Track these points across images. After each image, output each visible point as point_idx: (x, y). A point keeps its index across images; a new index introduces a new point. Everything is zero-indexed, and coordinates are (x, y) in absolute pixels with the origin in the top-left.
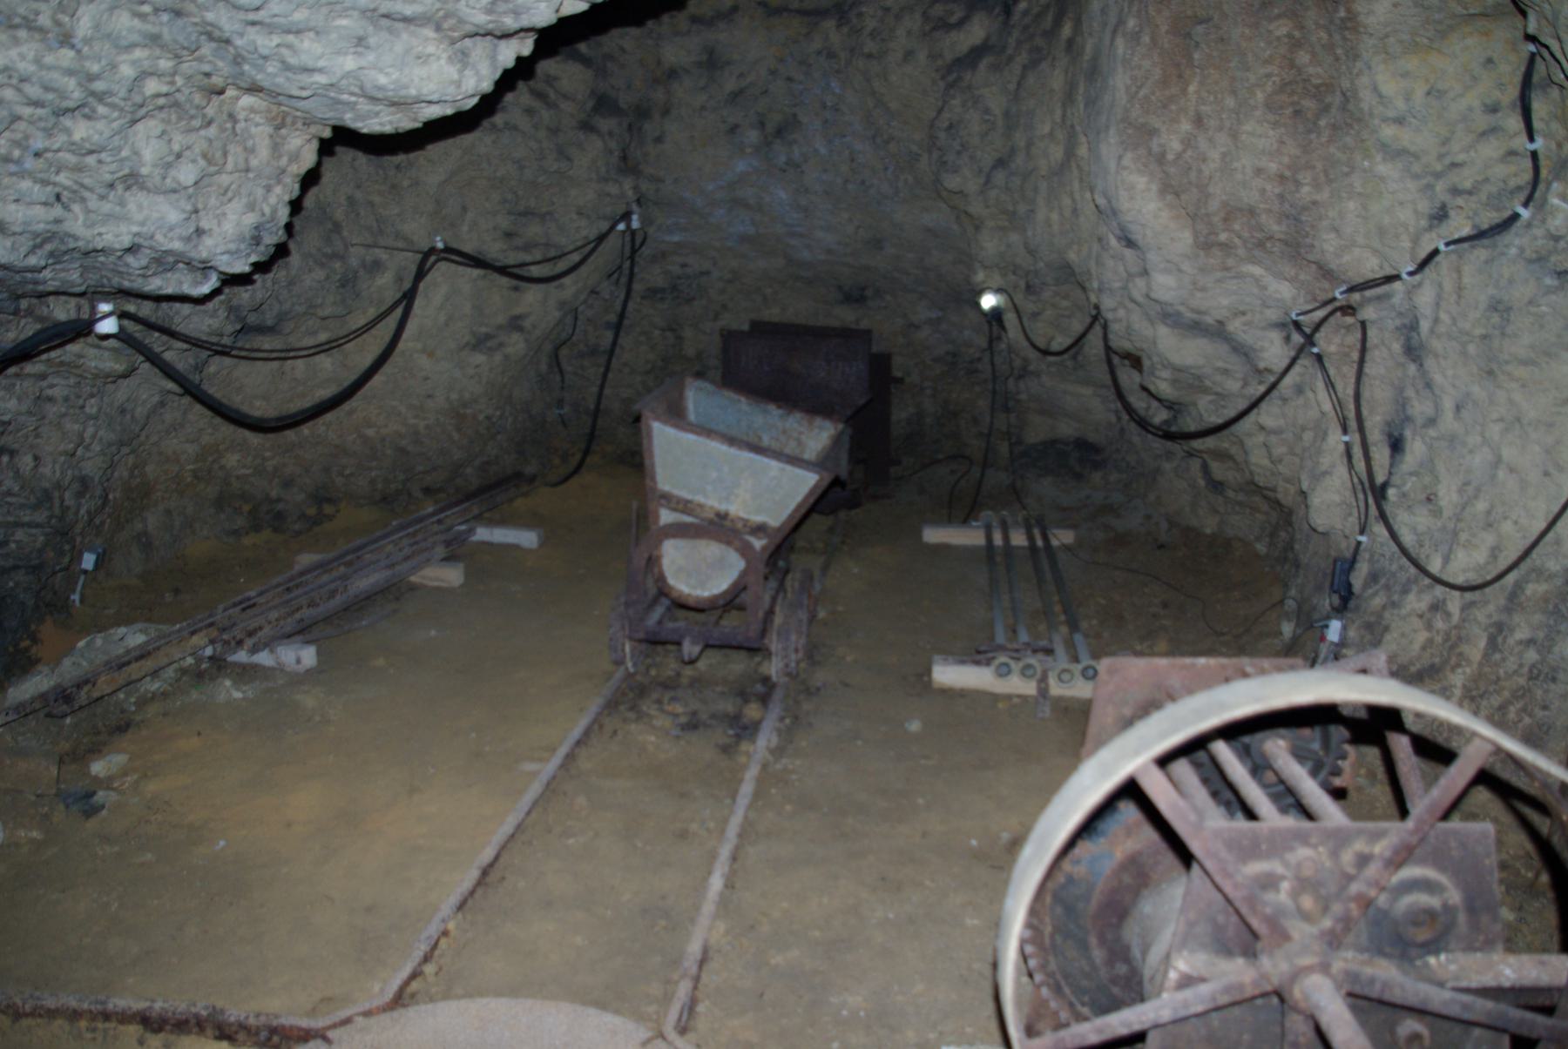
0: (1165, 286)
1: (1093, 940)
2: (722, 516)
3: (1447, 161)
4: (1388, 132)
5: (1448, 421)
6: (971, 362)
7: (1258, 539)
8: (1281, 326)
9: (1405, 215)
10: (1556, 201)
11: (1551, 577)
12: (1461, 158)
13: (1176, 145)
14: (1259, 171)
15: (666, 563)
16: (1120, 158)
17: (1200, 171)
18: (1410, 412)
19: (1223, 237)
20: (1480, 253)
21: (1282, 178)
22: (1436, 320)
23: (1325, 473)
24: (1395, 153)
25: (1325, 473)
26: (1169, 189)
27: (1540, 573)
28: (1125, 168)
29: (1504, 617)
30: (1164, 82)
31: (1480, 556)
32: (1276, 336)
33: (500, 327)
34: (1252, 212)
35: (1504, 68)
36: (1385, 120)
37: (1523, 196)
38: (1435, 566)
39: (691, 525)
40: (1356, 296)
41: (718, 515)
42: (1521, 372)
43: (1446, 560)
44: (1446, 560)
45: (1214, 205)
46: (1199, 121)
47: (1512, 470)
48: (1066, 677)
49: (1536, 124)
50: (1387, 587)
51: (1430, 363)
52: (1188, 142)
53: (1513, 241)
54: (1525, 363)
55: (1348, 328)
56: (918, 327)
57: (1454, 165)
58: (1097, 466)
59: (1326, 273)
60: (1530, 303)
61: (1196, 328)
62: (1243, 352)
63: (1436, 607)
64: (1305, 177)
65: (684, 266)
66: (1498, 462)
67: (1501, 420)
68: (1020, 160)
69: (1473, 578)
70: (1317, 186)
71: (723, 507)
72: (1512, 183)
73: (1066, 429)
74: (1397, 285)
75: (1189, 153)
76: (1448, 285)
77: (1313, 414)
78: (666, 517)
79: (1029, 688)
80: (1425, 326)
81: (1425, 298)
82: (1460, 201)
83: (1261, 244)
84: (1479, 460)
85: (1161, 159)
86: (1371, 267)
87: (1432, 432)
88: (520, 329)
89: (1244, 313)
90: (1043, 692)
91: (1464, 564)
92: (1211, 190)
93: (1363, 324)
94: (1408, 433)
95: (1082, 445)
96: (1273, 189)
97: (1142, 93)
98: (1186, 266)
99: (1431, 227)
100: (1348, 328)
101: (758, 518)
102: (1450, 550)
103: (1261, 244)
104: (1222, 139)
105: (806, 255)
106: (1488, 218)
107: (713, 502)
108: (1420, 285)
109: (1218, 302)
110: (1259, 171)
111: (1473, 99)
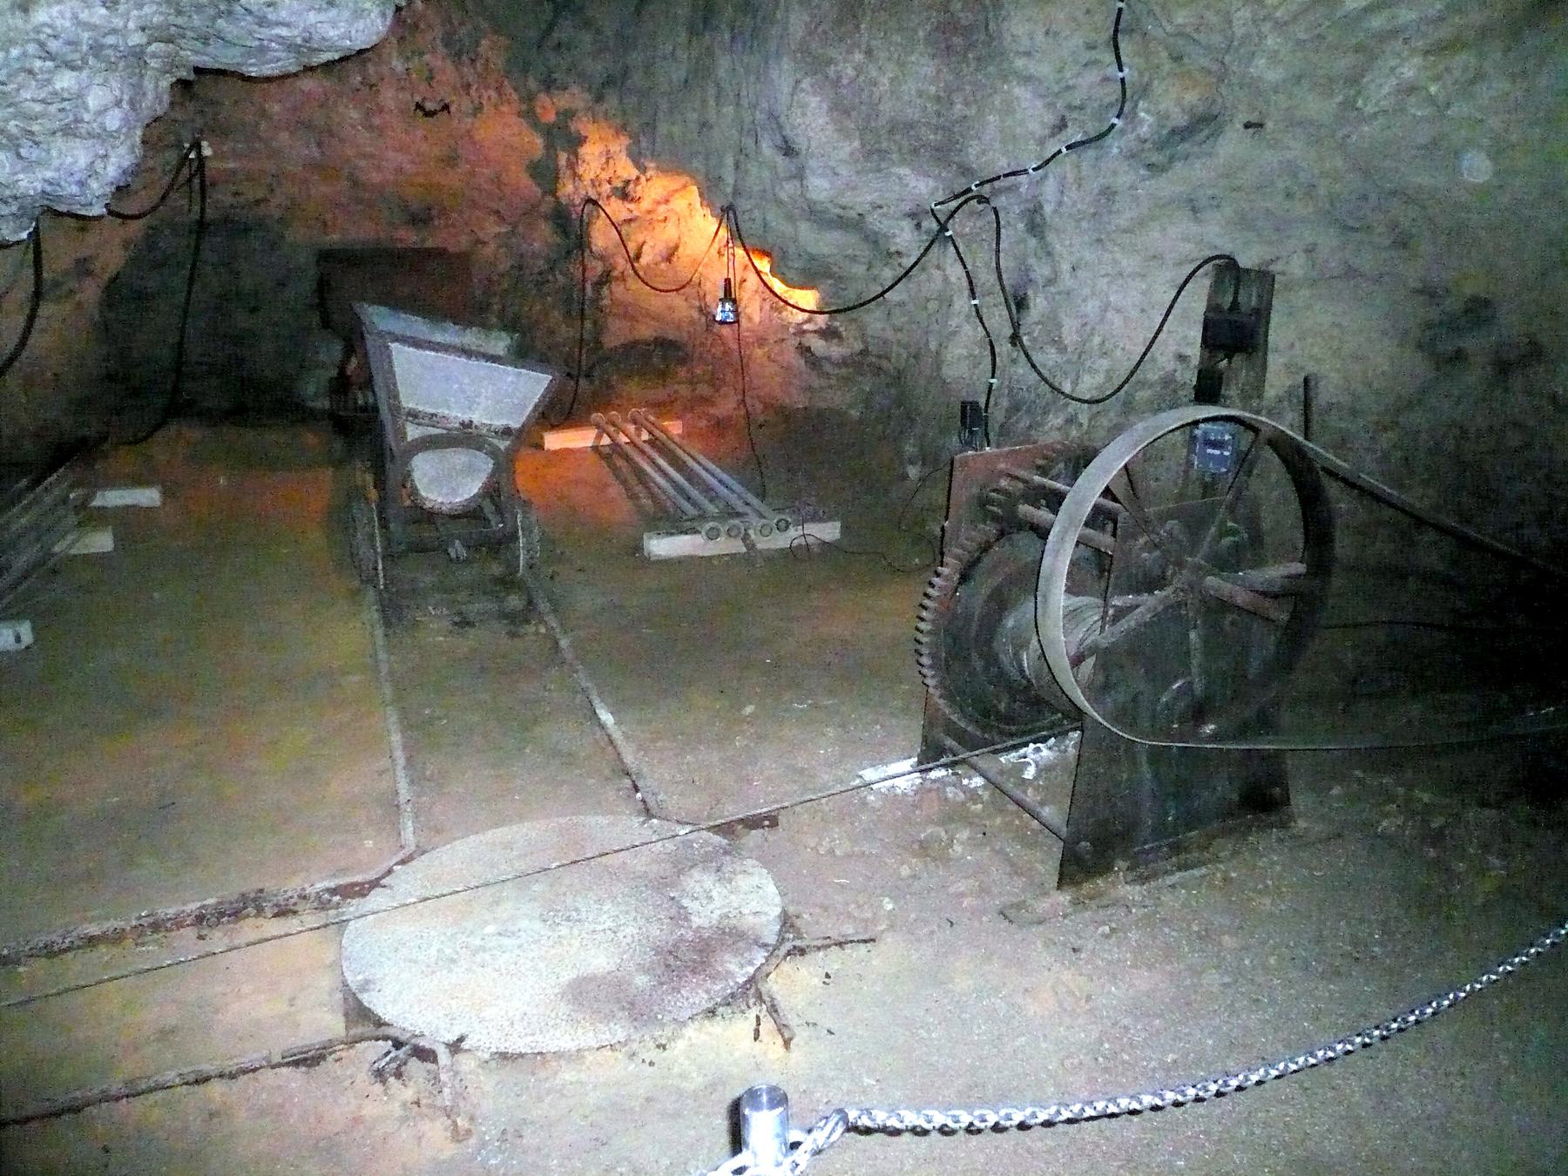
0: (819, 187)
1: (974, 656)
2: (467, 425)
3: (1063, 85)
4: (1020, 63)
5: (1067, 281)
6: (540, 273)
7: (851, 406)
8: (912, 215)
9: (1034, 126)
10: (1142, 114)
11: (1151, 385)
12: (1071, 83)
13: (850, 72)
14: (920, 94)
15: (416, 475)
16: (798, 82)
17: (872, 93)
18: (1033, 276)
19: (884, 145)
20: (1091, 153)
21: (938, 99)
22: (1060, 204)
23: (954, 333)
24: (1027, 79)
25: (954, 333)
26: (840, 109)
27: (1143, 384)
28: (803, 90)
29: (1122, 420)
30: (840, 22)
31: (1100, 378)
32: (907, 225)
33: (66, 273)
34: (910, 126)
35: (1099, 18)
36: (1018, 53)
37: (1115, 111)
38: (1067, 388)
39: (437, 436)
40: (987, 187)
41: (462, 424)
42: (1126, 238)
43: (1075, 383)
44: (1075, 383)
45: (882, 121)
46: (869, 52)
47: (1118, 311)
48: (766, 532)
49: (1123, 59)
50: (1028, 411)
51: (1051, 237)
52: (859, 69)
53: (1114, 145)
54: (1125, 231)
55: (980, 214)
56: (484, 243)
57: (1068, 88)
58: (683, 361)
59: (966, 171)
60: (1131, 188)
61: (841, 223)
62: (874, 240)
63: (1071, 421)
64: (958, 99)
65: (236, 194)
66: (1105, 308)
67: (1107, 275)
68: (637, 79)
69: (1096, 395)
70: (967, 104)
71: (466, 418)
72: (1107, 100)
73: (645, 331)
74: (1022, 178)
75: (862, 78)
76: (1070, 177)
77: (937, 284)
78: (413, 432)
79: (738, 547)
80: (1048, 209)
81: (1050, 189)
82: (1075, 115)
83: (915, 151)
84: (1092, 307)
85: (836, 83)
86: (1002, 164)
87: (1052, 289)
88: (89, 273)
89: (881, 207)
90: (751, 546)
91: (1088, 385)
92: (881, 107)
93: (996, 211)
94: (1030, 293)
95: (663, 344)
96: (931, 107)
97: (820, 30)
98: (843, 171)
99: (1053, 135)
100: (980, 214)
101: (499, 423)
102: (1078, 377)
103: (915, 151)
104: (891, 70)
105: (376, 177)
106: (1093, 129)
107: (456, 414)
108: (1045, 177)
109: (861, 199)
110: (920, 94)
111: (1077, 41)
